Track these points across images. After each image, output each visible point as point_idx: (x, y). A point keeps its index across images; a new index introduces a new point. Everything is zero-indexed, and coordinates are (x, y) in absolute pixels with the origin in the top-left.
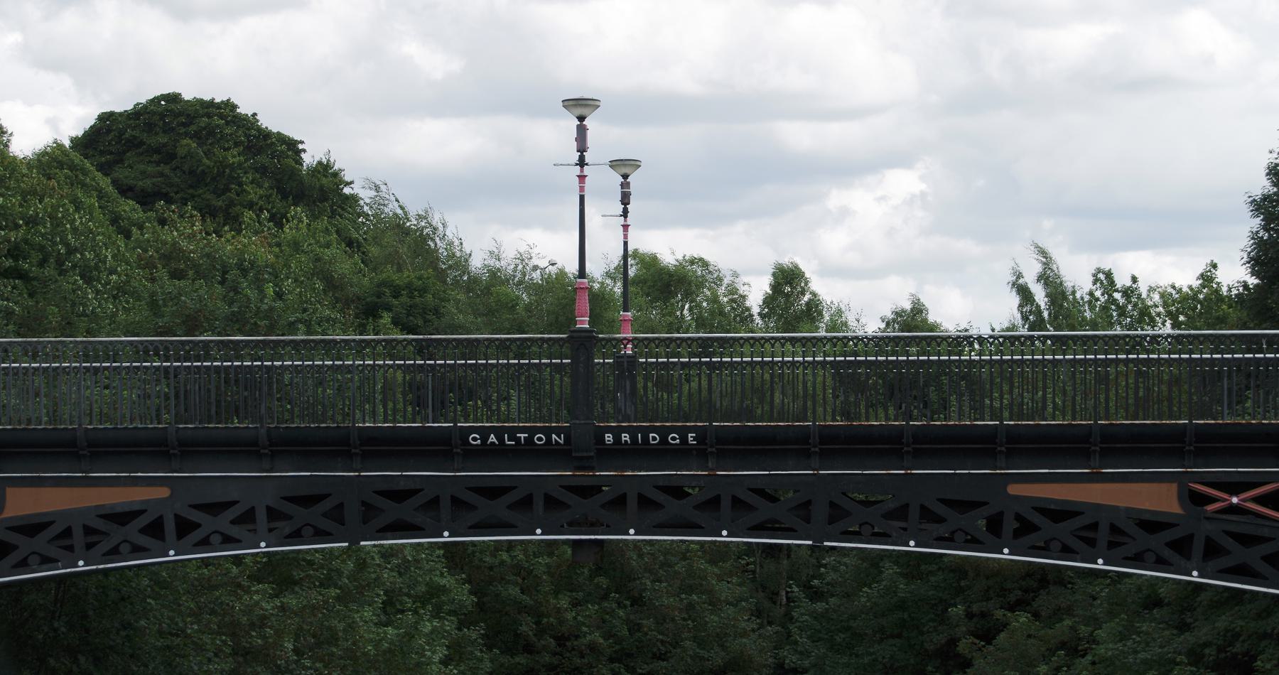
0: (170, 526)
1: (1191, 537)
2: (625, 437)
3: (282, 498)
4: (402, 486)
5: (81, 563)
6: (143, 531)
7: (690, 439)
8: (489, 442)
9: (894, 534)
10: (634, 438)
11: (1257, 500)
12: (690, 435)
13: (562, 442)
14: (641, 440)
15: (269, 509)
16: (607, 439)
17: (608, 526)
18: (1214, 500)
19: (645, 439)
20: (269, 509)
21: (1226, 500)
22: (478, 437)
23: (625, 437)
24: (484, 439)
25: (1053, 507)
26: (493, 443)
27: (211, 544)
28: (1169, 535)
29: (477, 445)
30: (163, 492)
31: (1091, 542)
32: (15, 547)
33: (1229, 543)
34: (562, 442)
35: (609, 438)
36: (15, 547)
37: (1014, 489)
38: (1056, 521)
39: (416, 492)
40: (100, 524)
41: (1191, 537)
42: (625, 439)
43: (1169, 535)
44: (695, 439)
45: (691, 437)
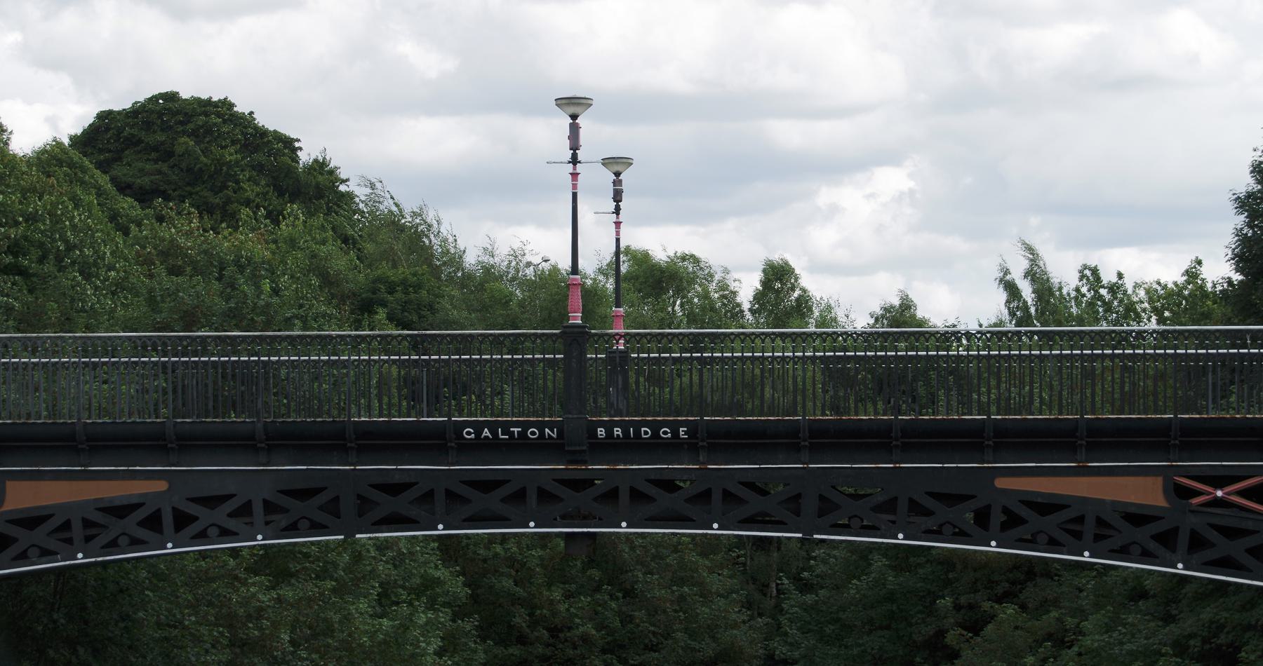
0: (168, 519)
1: (1176, 530)
2: (618, 431)
3: (278, 491)
4: (397, 479)
5: (80, 555)
6: (141, 524)
7: (681, 433)
8: (482, 436)
9: (883, 527)
10: (626, 433)
11: (1241, 493)
12: (681, 429)
13: (555, 436)
14: (633, 435)
15: (265, 502)
16: (599, 433)
17: (600, 519)
18: (1199, 493)
19: (637, 433)
20: (265, 502)
21: (1211, 493)
22: (472, 431)
23: (617, 431)
24: (478, 433)
25: (1039, 500)
26: (487, 437)
27: (208, 537)
28: (1154, 528)
29: (471, 439)
30: (161, 486)
31: (1078, 535)
32: (15, 540)
33: (1213, 536)
34: (555, 436)
35: (601, 432)
36: (15, 540)
37: (1001, 483)
38: (1043, 514)
39: (411, 485)
40: (98, 517)
41: (1176, 530)
42: (618, 433)
43: (1154, 528)
44: (686, 433)
45: (683, 431)
